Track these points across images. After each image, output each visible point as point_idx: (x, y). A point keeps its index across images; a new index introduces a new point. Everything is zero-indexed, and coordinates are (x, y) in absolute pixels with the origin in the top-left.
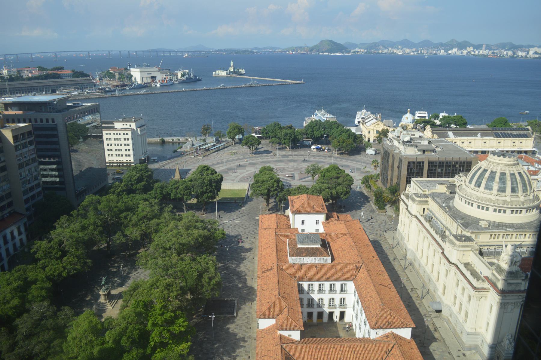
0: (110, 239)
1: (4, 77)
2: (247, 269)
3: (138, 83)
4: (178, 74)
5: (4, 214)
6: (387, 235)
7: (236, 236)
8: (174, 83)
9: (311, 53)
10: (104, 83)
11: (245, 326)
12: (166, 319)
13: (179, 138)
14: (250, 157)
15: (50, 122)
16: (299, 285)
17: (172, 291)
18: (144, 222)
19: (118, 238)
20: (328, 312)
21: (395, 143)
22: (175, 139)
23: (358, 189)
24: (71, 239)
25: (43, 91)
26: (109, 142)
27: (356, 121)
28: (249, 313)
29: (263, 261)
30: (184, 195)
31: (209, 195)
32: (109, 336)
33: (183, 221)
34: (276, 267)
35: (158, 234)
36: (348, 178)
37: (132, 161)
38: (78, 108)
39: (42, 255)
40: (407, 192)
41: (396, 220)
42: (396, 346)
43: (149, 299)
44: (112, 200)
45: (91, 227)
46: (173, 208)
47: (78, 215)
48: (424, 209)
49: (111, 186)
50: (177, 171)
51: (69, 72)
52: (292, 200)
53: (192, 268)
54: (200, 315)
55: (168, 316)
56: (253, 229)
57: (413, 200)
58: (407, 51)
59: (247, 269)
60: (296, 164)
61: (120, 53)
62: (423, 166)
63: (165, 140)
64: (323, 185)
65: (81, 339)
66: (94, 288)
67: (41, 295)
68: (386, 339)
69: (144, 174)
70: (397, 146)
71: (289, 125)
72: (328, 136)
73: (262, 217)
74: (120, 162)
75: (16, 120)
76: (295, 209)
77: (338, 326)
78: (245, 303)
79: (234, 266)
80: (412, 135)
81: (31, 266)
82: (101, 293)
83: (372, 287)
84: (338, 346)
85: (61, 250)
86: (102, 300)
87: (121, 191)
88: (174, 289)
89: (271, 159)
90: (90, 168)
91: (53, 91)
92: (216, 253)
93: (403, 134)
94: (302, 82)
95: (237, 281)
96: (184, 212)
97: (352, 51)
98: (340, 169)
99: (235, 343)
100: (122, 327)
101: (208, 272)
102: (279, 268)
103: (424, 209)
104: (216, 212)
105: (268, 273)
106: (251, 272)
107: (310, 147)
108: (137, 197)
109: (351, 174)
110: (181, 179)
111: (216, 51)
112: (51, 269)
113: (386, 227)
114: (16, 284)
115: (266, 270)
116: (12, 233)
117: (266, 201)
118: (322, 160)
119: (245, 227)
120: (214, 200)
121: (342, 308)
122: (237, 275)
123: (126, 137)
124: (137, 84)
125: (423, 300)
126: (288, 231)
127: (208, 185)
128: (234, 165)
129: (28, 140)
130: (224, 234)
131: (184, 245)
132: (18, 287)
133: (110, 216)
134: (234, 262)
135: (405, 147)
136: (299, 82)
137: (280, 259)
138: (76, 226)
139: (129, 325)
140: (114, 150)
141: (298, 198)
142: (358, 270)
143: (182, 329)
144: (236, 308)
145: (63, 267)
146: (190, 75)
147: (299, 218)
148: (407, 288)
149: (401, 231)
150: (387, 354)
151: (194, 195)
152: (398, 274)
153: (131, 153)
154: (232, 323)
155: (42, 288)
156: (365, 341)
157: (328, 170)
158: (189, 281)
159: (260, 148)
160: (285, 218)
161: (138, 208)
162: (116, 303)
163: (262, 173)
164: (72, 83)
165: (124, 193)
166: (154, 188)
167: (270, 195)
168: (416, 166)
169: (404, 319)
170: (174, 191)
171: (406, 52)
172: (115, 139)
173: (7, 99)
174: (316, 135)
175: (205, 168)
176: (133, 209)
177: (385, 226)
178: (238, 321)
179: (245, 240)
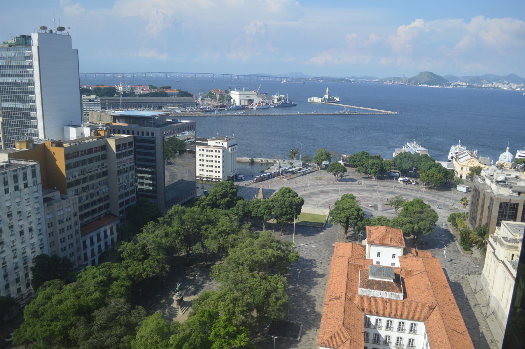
0: (190, 249)
1: (119, 93)
2: (317, 295)
3: (237, 105)
4: (274, 98)
5: (101, 214)
6: (470, 278)
7: (311, 261)
8: (269, 107)
9: (409, 84)
10: (205, 103)
12: (228, 332)
13: (267, 159)
14: (334, 184)
15: (150, 135)
17: (239, 306)
18: (222, 236)
19: (197, 248)
21: (488, 182)
22: (264, 160)
23: (444, 227)
24: (153, 244)
25: (151, 107)
26: (202, 158)
27: (450, 156)
28: (313, 339)
29: (332, 288)
30: (264, 214)
31: (288, 217)
33: (260, 239)
34: (344, 296)
36: (433, 213)
37: (221, 177)
38: (176, 125)
39: (127, 255)
40: (495, 235)
41: (481, 264)
43: (216, 310)
44: (196, 212)
45: (174, 235)
46: (252, 226)
47: (164, 222)
48: (513, 255)
50: (261, 191)
51: (176, 91)
52: (370, 231)
53: (261, 285)
54: (264, 334)
55: (231, 329)
56: (328, 256)
57: (501, 244)
58: (514, 86)
59: (317, 295)
60: (381, 195)
61: (223, 76)
62: (517, 209)
63: (255, 160)
64: (405, 218)
65: (147, 338)
66: (169, 292)
67: (120, 292)
69: (229, 190)
70: (489, 184)
71: (377, 155)
72: (417, 169)
73: (337, 244)
74: (210, 177)
75: (121, 131)
76: (371, 240)
78: (310, 329)
79: (304, 289)
80: (507, 175)
81: (116, 264)
82: (174, 298)
83: (445, 331)
85: (144, 253)
86: (175, 305)
88: (240, 305)
89: (355, 188)
90: (182, 180)
91: (160, 108)
92: (288, 274)
93: (497, 173)
94: (396, 113)
95: (305, 306)
97: (453, 84)
100: (186, 333)
101: (276, 292)
102: (347, 298)
103: (513, 255)
104: (294, 234)
105: (335, 301)
106: (320, 299)
107: (397, 178)
108: (219, 212)
109: (437, 211)
110: (264, 198)
111: (314, 78)
112: (132, 269)
113: (470, 270)
114: (100, 279)
115: (334, 299)
116: (105, 232)
118: (408, 193)
119: (320, 253)
122: (306, 300)
123: (218, 154)
124: (235, 106)
126: (362, 261)
127: (288, 207)
128: (317, 190)
129: (129, 150)
130: (297, 257)
131: (256, 262)
132: (101, 281)
133: (192, 227)
134: (305, 286)
135: (498, 186)
136: (393, 113)
137: (350, 288)
138: (160, 232)
139: (192, 332)
140: (205, 166)
141: (376, 229)
142: (431, 311)
143: (243, 343)
144: (300, 332)
145: (143, 269)
146: (285, 100)
148: (487, 338)
149: (486, 276)
151: (273, 215)
153: (221, 169)
155: (122, 286)
157: (412, 204)
158: (256, 298)
159: (346, 176)
160: (361, 247)
161: (219, 222)
162: (187, 310)
163: (343, 201)
164: (177, 101)
165: (209, 207)
166: (237, 205)
167: (349, 223)
168: (509, 208)
170: (255, 209)
171: (513, 88)
172: (207, 156)
173: (116, 112)
174: (404, 167)
175: (287, 191)
177: (468, 268)
179: (319, 265)
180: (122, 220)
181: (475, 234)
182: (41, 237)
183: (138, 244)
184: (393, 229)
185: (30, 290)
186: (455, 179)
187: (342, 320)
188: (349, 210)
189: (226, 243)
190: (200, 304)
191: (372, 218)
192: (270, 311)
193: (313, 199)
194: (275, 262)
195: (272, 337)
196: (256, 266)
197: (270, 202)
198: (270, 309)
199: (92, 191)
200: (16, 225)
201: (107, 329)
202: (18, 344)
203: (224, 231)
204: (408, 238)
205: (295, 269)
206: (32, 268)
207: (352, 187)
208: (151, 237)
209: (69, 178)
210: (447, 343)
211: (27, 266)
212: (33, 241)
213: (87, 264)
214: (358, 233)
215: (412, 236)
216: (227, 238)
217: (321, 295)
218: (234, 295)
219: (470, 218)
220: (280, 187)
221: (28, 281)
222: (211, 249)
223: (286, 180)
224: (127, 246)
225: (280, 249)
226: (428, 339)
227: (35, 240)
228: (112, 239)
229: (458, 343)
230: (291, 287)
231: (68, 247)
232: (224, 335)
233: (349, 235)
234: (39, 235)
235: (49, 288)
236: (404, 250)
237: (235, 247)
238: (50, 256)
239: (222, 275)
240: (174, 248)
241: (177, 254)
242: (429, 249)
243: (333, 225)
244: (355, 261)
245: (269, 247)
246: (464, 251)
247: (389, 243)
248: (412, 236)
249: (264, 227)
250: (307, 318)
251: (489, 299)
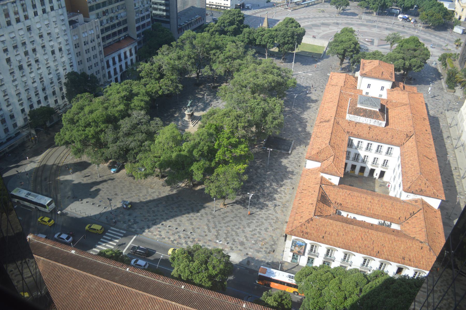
0: (200, 71)
5: (120, 36)
6: (448, 114)
7: (306, 87)
11: (296, 164)
12: (230, 142)
14: (336, 17)
16: (350, 139)
17: (241, 122)
18: (229, 61)
19: (206, 71)
20: (370, 169)
23: (433, 65)
28: (302, 153)
30: (268, 42)
31: (289, 46)
32: (185, 146)
33: (262, 65)
34: (333, 120)
35: (239, 73)
36: (426, 52)
37: (229, 5)
39: (145, 74)
42: (421, 211)
43: (222, 124)
45: (186, 58)
46: (255, 53)
47: (177, 46)
49: (208, 25)
50: (266, 20)
52: (364, 64)
54: (261, 146)
55: (233, 140)
60: (379, 30)
64: (398, 54)
66: (182, 108)
68: (414, 203)
69: (236, 18)
72: (418, 7)
74: (219, 5)
76: (364, 72)
77: (376, 182)
78: (300, 145)
79: (298, 112)
81: (136, 82)
82: (186, 112)
83: (416, 156)
84: (369, 198)
85: (160, 73)
86: (186, 118)
87: (214, 31)
88: (242, 121)
89: (356, 22)
90: (192, 7)
92: (285, 98)
95: (298, 126)
96: (265, 58)
98: (419, 42)
99: (284, 175)
100: (196, 141)
101: (274, 112)
102: (335, 122)
104: (293, 62)
105: (325, 124)
106: (312, 121)
107: (397, 15)
108: (226, 38)
109: (430, 49)
113: (450, 106)
114: (123, 94)
115: (324, 121)
116: (125, 53)
117: (340, 60)
119: (316, 81)
120: (294, 52)
121: (384, 168)
122: (299, 121)
125: (463, 180)
126: (353, 91)
127: (290, 37)
128: (319, 22)
130: (295, 83)
131: (258, 86)
132: (124, 96)
133: (202, 51)
134: (299, 109)
137: (339, 113)
138: (174, 55)
139: (201, 141)
141: (370, 62)
143: (243, 153)
144: (292, 147)
145: (159, 87)
147: (366, 81)
148: (452, 165)
150: (411, 215)
151: (276, 43)
152: (447, 151)
154: (286, 158)
156: (395, 199)
157: (407, 41)
160: (354, 79)
161: (226, 47)
162: (197, 123)
163: (342, 34)
165: (217, 33)
166: (243, 32)
167: (346, 55)
169: (437, 191)
170: (260, 37)
174: (406, 5)
175: (291, 21)
176: (222, 48)
177: (448, 105)
178: (291, 158)
180: (139, 43)
181: (461, 75)
182: (70, 56)
183: (154, 65)
184: (386, 64)
185: (65, 101)
186: (454, 20)
187: (329, 140)
188: (347, 43)
189: (232, 67)
190: (208, 119)
191: (367, 52)
192: (267, 128)
193: (314, 30)
194: (275, 86)
195: (268, 149)
196: (258, 89)
197: (274, 31)
198: (267, 126)
199: (112, 15)
200: (48, 45)
201: (131, 135)
202: (60, 144)
203: (230, 57)
204: (398, 73)
205: (291, 94)
206: (65, 83)
207: (352, 21)
208: (166, 59)
209: (90, 2)
210: (417, 166)
211: (61, 81)
212: (63, 59)
213: (111, 81)
214: (352, 65)
215: (402, 72)
216: (233, 63)
217: (313, 118)
218: (238, 113)
219: (460, 59)
220: (284, 17)
221: (63, 94)
222: (218, 72)
223: (290, 11)
224: (145, 67)
225: (280, 75)
226: (401, 162)
227: (65, 59)
228: (132, 60)
229: (426, 167)
230: (287, 109)
231: (94, 66)
232: (227, 144)
233: (344, 67)
234: (68, 54)
235: (82, 100)
236: (393, 84)
237: (239, 71)
238: (79, 73)
239: (227, 96)
240: (186, 69)
241: (189, 75)
242: (416, 84)
243: (330, 56)
244: (346, 90)
245: (270, 73)
246: (448, 89)
247: (380, 76)
248: (402, 72)
249: (266, 54)
250: (298, 135)
251: (462, 133)
